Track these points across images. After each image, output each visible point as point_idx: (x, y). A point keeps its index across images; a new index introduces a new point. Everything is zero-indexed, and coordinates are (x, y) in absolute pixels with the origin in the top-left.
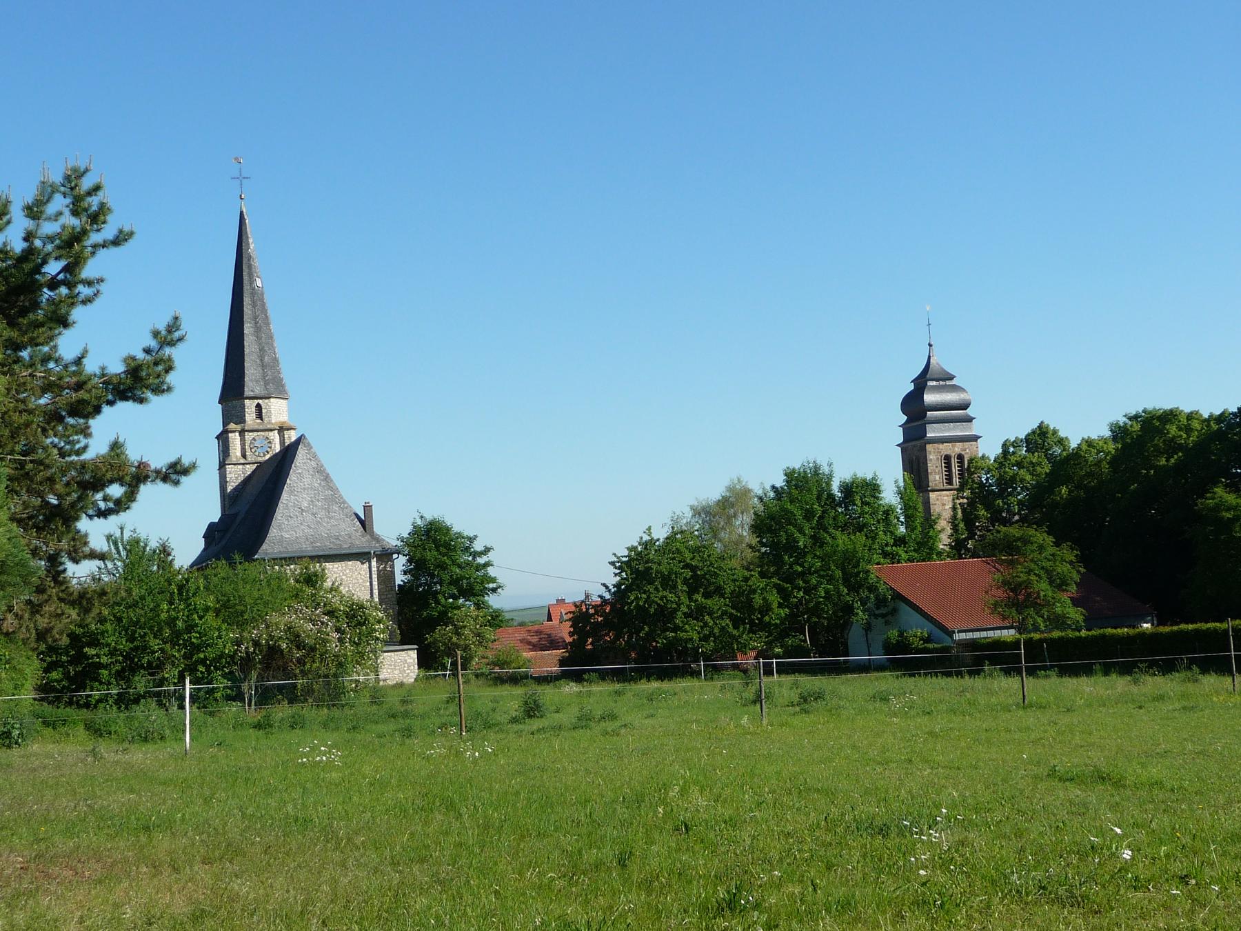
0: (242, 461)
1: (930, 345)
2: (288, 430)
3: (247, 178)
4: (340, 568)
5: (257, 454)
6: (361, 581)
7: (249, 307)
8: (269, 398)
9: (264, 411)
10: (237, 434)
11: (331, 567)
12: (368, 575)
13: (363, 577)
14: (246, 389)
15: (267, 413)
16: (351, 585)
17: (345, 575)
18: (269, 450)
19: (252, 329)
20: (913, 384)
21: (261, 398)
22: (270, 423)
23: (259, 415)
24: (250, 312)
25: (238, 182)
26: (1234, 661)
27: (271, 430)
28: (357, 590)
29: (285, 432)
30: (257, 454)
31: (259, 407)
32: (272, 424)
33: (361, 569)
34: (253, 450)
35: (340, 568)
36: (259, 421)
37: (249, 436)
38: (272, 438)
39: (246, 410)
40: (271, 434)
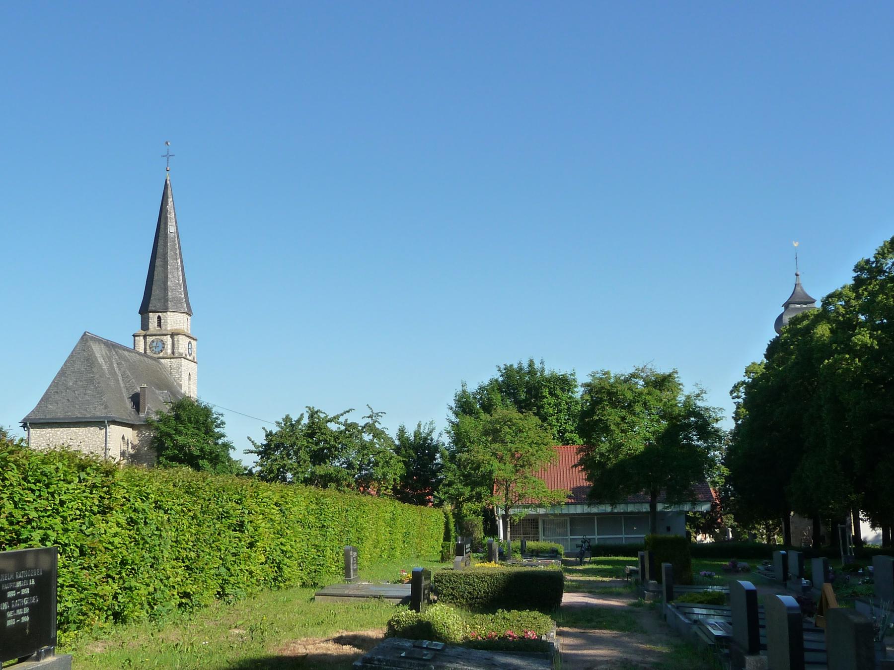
0: (172, 356)
1: (797, 275)
2: (177, 334)
3: (164, 156)
4: (84, 433)
5: (154, 352)
6: (99, 443)
7: (162, 247)
8: (166, 312)
9: (162, 321)
10: (169, 336)
11: (77, 431)
12: (104, 439)
13: (100, 440)
14: (150, 305)
15: (164, 322)
16: (91, 446)
17: (88, 438)
18: (163, 349)
19: (161, 263)
20: (783, 307)
21: (161, 312)
22: (166, 329)
23: (159, 325)
25: (165, 158)
26: (570, 559)
27: (165, 335)
29: (175, 336)
30: (154, 352)
31: (159, 317)
32: (167, 330)
34: (151, 349)
35: (84, 433)
36: (159, 328)
37: (149, 339)
38: (165, 340)
39: (150, 320)
40: (165, 337)
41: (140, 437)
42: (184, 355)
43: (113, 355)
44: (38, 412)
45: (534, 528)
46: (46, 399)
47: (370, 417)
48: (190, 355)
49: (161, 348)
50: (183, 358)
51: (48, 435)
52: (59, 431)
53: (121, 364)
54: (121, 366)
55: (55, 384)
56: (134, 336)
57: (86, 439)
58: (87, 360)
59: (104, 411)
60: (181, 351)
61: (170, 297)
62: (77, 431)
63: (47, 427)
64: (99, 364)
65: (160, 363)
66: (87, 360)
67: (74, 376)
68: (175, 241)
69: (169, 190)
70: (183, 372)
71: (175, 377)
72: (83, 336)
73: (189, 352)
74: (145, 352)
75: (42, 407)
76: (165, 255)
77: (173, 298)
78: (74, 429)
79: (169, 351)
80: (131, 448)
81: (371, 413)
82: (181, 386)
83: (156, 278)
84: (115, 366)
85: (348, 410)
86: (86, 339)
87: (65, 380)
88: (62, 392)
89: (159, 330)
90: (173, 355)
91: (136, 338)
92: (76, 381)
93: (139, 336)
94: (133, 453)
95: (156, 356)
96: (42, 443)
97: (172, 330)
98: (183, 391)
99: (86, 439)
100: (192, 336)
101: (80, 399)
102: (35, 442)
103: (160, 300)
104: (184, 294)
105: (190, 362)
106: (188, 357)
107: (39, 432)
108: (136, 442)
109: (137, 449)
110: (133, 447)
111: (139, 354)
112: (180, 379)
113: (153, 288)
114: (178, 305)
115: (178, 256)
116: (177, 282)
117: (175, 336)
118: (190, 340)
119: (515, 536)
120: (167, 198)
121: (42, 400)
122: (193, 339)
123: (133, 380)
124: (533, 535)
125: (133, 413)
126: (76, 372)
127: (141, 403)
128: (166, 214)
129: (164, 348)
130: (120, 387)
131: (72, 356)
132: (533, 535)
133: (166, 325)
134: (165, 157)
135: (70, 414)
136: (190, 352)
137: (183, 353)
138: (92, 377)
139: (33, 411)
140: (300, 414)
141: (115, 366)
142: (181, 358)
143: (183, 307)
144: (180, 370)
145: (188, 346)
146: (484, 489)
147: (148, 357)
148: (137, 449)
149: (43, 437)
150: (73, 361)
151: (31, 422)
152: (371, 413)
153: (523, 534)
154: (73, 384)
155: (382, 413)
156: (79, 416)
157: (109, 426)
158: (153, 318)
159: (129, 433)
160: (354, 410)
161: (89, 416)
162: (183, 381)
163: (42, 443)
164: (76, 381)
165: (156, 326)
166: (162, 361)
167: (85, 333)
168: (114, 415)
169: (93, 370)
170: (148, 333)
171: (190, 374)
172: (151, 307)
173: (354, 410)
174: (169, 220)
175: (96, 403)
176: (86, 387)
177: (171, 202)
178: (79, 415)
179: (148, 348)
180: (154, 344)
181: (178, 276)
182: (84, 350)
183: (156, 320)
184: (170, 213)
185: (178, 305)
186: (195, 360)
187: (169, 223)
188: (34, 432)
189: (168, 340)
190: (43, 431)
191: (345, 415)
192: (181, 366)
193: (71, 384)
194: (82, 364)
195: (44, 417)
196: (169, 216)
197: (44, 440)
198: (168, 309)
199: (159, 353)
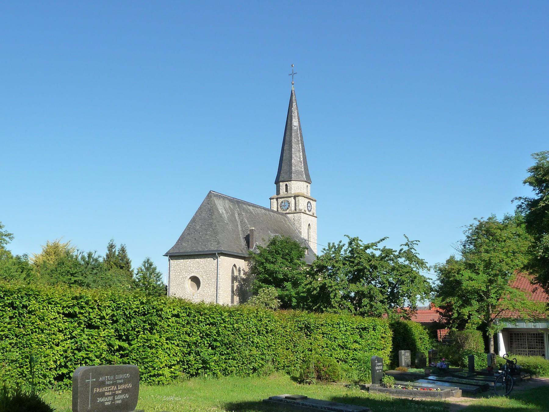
0: (295, 212)
2: (298, 196)
3: (295, 73)
6: (213, 269)
9: (288, 188)
10: (292, 198)
11: (199, 261)
15: (289, 188)
16: (208, 272)
18: (289, 207)
21: (287, 181)
23: (287, 191)
24: (288, 139)
27: (290, 197)
28: (211, 274)
29: (297, 198)
31: (286, 185)
32: (292, 194)
33: (213, 263)
34: (281, 208)
38: (290, 201)
40: (290, 199)
41: (250, 266)
42: (303, 211)
43: (236, 208)
44: (176, 248)
45: (539, 343)
46: (182, 239)
47: (407, 244)
48: (310, 211)
49: (287, 207)
50: (302, 213)
51: (181, 264)
52: (188, 261)
53: (241, 214)
54: (240, 216)
55: (188, 228)
56: (270, 199)
57: (205, 267)
58: (210, 210)
59: (217, 246)
60: (301, 208)
61: (294, 170)
62: (199, 261)
63: (181, 258)
64: (219, 213)
65: (287, 217)
66: (210, 210)
67: (201, 222)
68: (297, 131)
69: (293, 97)
70: (302, 223)
71: (297, 227)
72: (209, 193)
73: (308, 209)
74: (278, 210)
75: (179, 244)
76: (291, 141)
77: (296, 171)
78: (198, 259)
79: (293, 208)
80: (244, 274)
81: (407, 241)
82: (301, 233)
83: (284, 158)
84: (237, 215)
85: (383, 238)
86: (210, 195)
87: (195, 225)
88: (192, 233)
89: (286, 194)
90: (296, 212)
91: (271, 200)
92: (202, 226)
93: (273, 199)
94: (245, 278)
95: (284, 212)
96: (178, 270)
97: (295, 193)
98: (302, 237)
99: (205, 267)
100: (311, 198)
101: (203, 238)
102: (173, 269)
103: (286, 173)
104: (305, 168)
105: (309, 216)
106: (307, 212)
107: (176, 262)
108: (247, 270)
109: (248, 275)
110: (245, 274)
111: (273, 211)
112: (300, 227)
113: (282, 166)
114: (299, 176)
115: (300, 142)
116: (299, 160)
117: (297, 198)
118: (310, 201)
119: (520, 350)
120: (292, 102)
121: (179, 239)
122: (312, 200)
123: (248, 225)
124: (538, 350)
125: (245, 249)
126: (202, 219)
127: (250, 241)
128: (291, 113)
129: (289, 206)
130: (238, 230)
131: (200, 208)
132: (538, 350)
133: (291, 190)
134: (291, 75)
135: (195, 248)
136: (310, 209)
137: (302, 210)
138: (211, 222)
139: (173, 248)
140: (339, 241)
141: (237, 215)
142: (300, 213)
143: (303, 177)
144: (300, 221)
145: (308, 205)
146: (454, 300)
147: (279, 213)
148: (248, 275)
149: (178, 266)
150: (201, 211)
151: (170, 255)
152: (407, 241)
153: (528, 348)
154: (200, 227)
155: (416, 241)
156: (200, 250)
157: (219, 257)
158: (282, 185)
159: (242, 264)
160: (388, 238)
161: (206, 250)
162: (302, 229)
163: (178, 270)
164: (202, 226)
165: (285, 191)
166: (288, 215)
167: (210, 191)
168: (223, 249)
169: (213, 217)
170: (279, 197)
171: (309, 225)
172: (281, 179)
173: (388, 238)
174: (293, 118)
175: (212, 241)
176: (208, 229)
177: (295, 105)
178: (200, 250)
179: (279, 207)
180: (283, 204)
181: (299, 156)
182: (209, 204)
183: (284, 187)
184: (294, 113)
185: (299, 176)
186: (315, 215)
187: (294, 120)
188: (173, 262)
189: (292, 200)
190: (178, 261)
191: (381, 242)
192: (301, 218)
193: (198, 228)
194: (206, 214)
195: (179, 251)
196: (293, 115)
197: (179, 268)
198: (292, 178)
199: (286, 210)
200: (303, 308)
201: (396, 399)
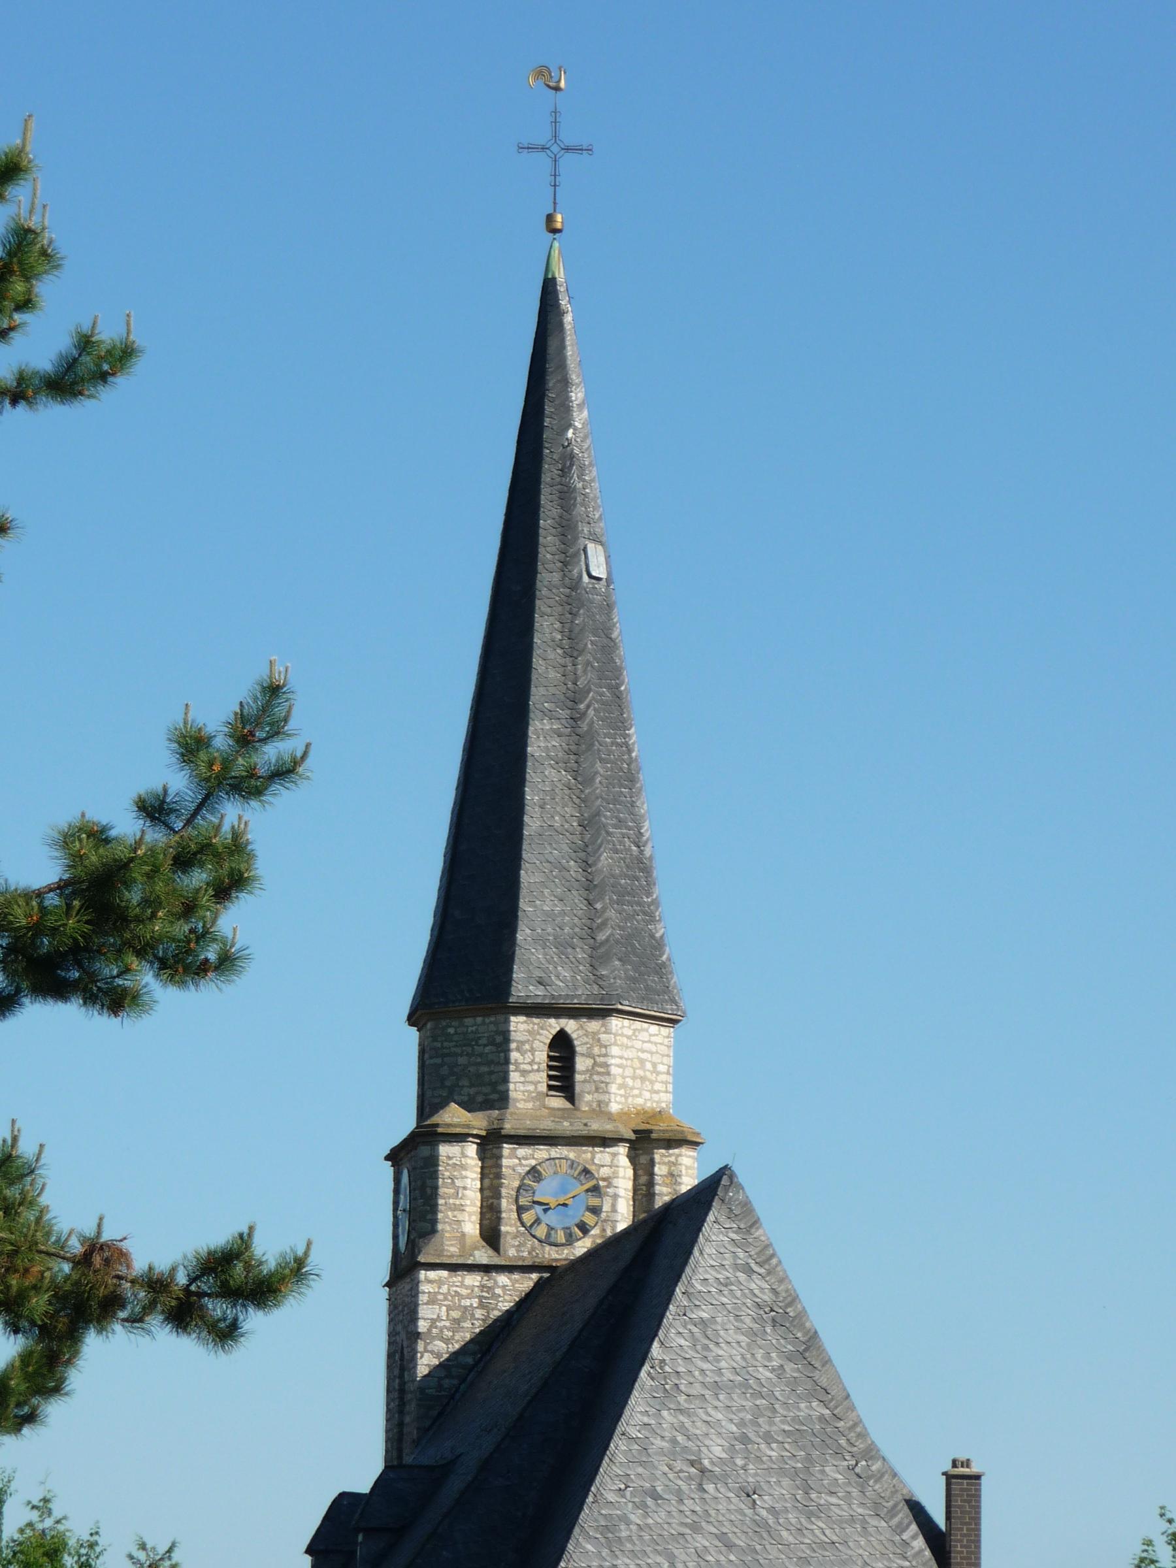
0: (483, 1256)
3: (578, 150)
9: (581, 1064)
15: (591, 1071)
18: (589, 1219)
27: (605, 1141)
29: (659, 1155)
31: (562, 1046)
32: (610, 1117)
34: (528, 1217)
38: (604, 1172)
40: (602, 1156)
89: (562, 1114)
117: (659, 1155)
133: (601, 1088)
179: (507, 1205)
199: (570, 1240)
200: (626, 736)
201: (612, 1146)
